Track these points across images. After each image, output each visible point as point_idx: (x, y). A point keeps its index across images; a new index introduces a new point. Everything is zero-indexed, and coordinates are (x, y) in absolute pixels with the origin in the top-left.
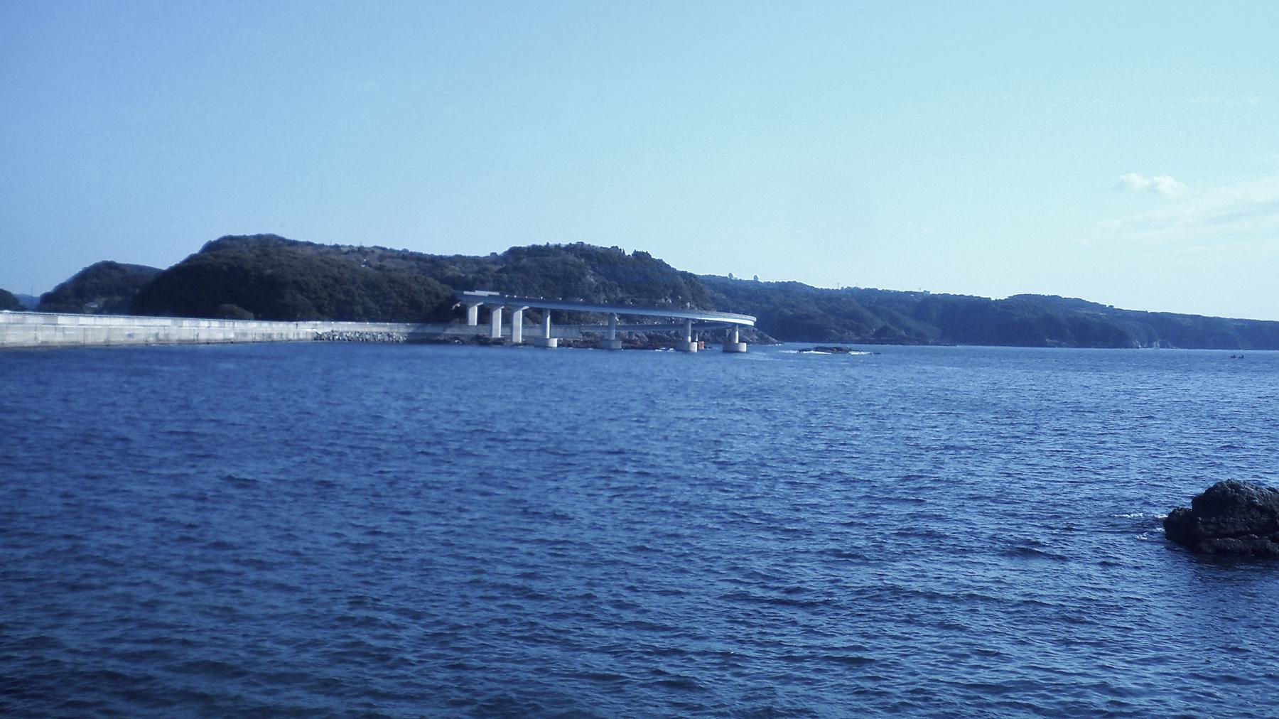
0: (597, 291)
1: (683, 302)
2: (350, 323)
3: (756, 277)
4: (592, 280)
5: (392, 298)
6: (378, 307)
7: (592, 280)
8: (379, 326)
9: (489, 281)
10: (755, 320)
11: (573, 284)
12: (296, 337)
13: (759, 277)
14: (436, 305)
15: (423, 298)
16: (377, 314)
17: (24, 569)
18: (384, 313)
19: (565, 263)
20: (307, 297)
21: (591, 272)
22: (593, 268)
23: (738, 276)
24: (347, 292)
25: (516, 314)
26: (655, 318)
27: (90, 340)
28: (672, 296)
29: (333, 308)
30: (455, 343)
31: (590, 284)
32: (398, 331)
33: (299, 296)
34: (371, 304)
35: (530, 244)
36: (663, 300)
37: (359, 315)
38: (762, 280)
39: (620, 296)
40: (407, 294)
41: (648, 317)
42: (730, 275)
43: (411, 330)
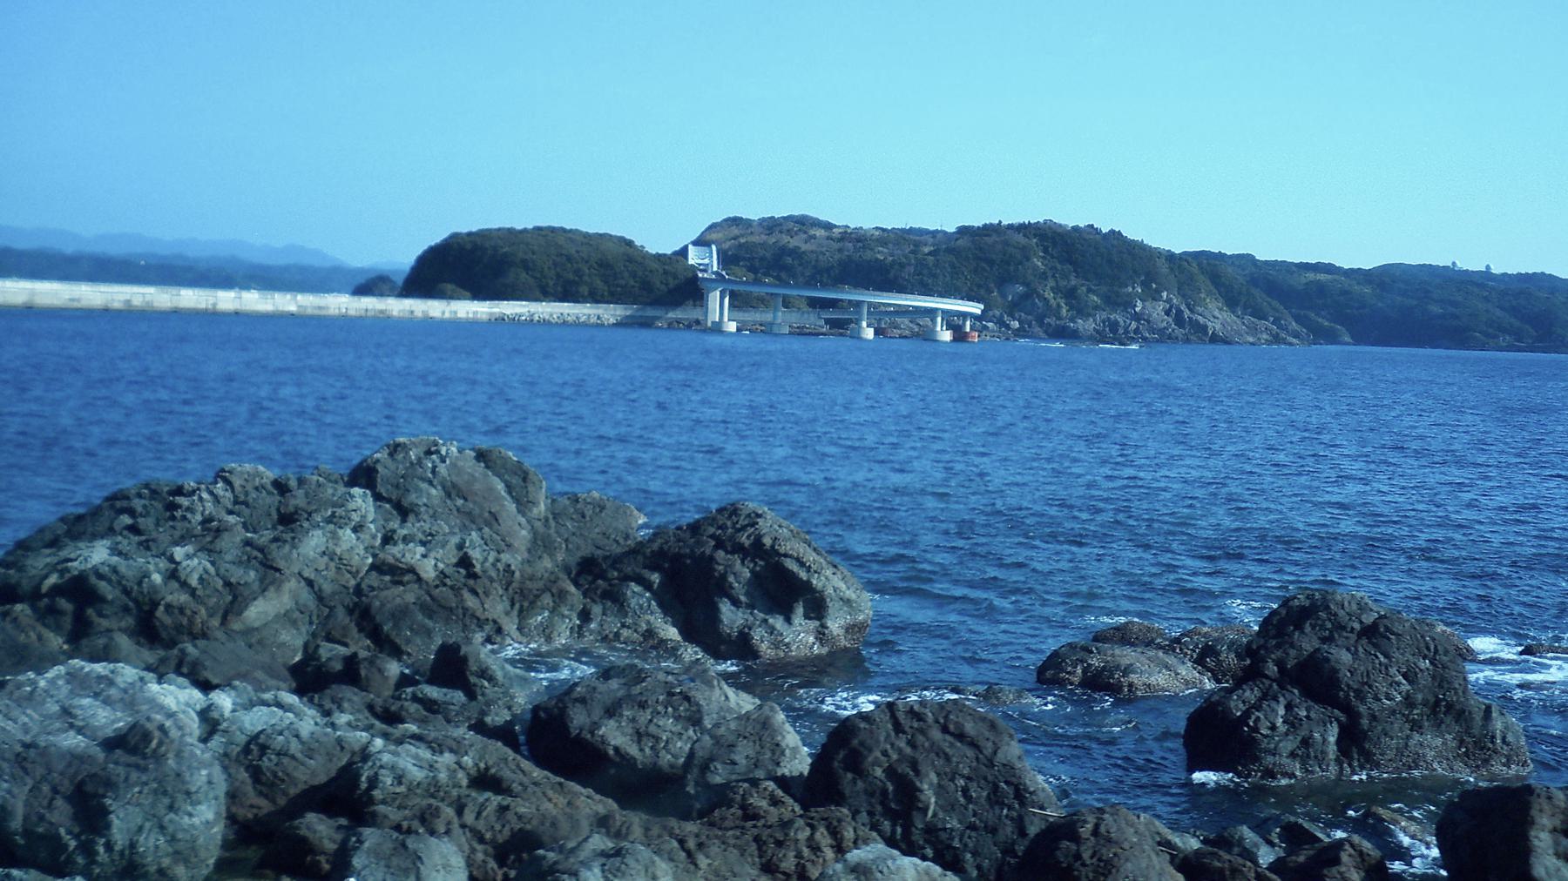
0: (1044, 276)
1: (1159, 292)
2: (566, 304)
3: (1488, 267)
4: (1040, 264)
5: (623, 278)
6: (606, 288)
7: (1040, 264)
8: (521, 305)
9: (909, 265)
10: (982, 307)
11: (1012, 268)
12: (337, 311)
13: (1492, 267)
14: (671, 286)
15: (656, 282)
16: (602, 296)
17: (651, 435)
18: (612, 294)
19: (1006, 243)
20: (532, 276)
21: (1041, 254)
22: (1045, 251)
23: (1463, 265)
24: (578, 272)
25: (711, 295)
26: (890, 305)
27: (84, 304)
28: (1143, 284)
29: (559, 289)
30: (680, 329)
31: (1036, 268)
32: (610, 313)
33: (524, 275)
34: (599, 283)
35: (1138, 238)
36: (1131, 289)
37: (583, 296)
38: (1496, 270)
39: (1073, 283)
40: (640, 273)
41: (884, 304)
42: (1454, 263)
43: (628, 313)
